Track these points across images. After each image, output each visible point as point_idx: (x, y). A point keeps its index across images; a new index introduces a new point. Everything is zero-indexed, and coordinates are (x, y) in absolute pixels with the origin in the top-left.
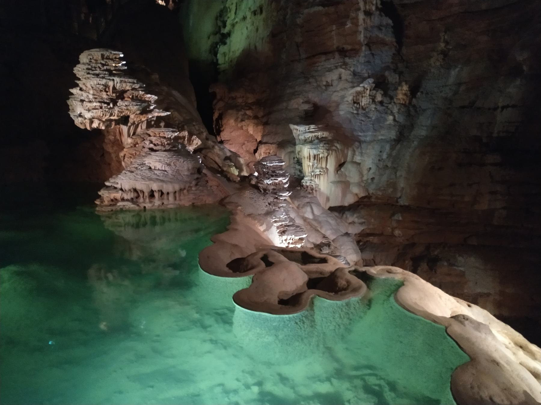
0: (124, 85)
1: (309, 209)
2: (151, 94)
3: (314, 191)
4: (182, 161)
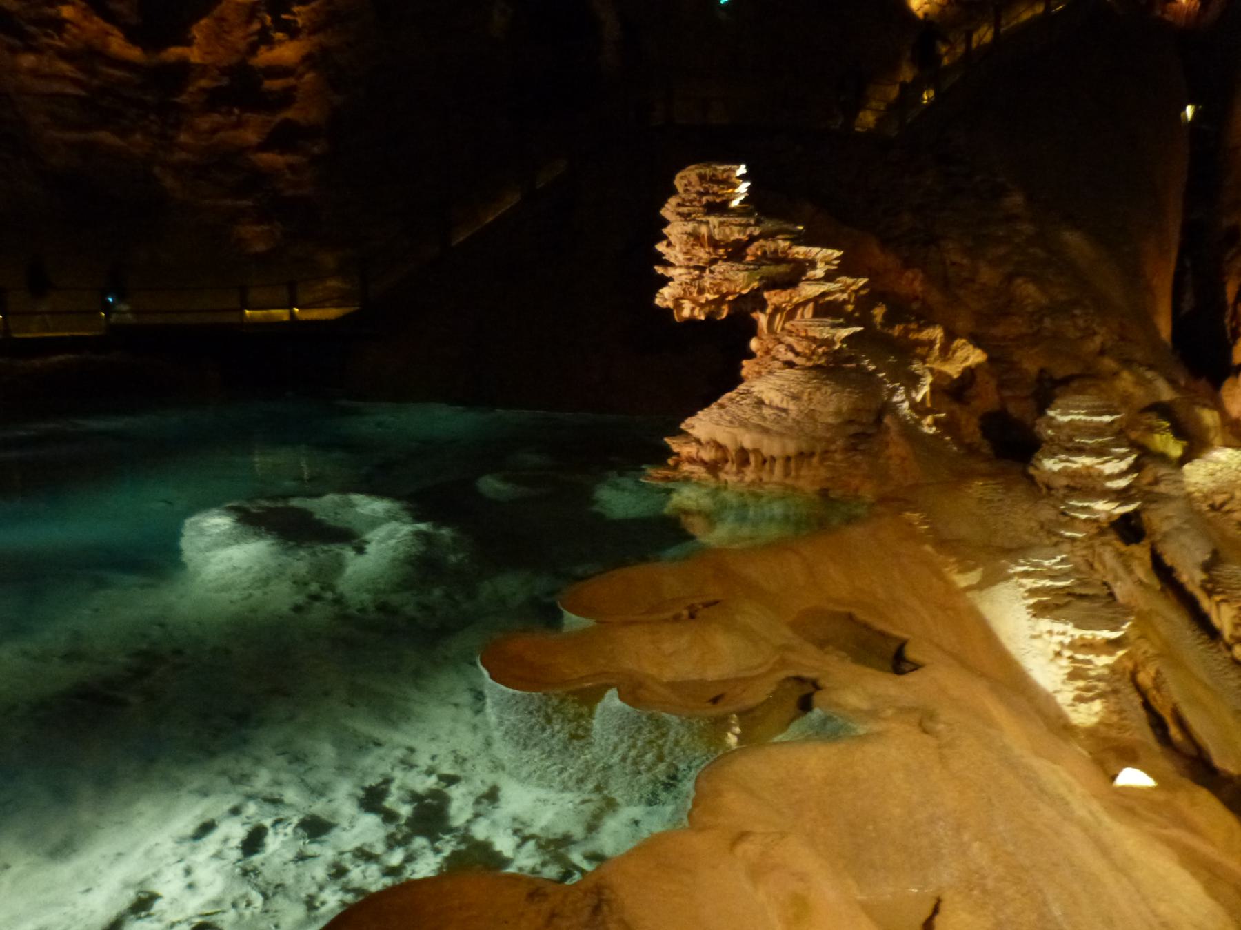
0: (727, 231)
4: (829, 391)
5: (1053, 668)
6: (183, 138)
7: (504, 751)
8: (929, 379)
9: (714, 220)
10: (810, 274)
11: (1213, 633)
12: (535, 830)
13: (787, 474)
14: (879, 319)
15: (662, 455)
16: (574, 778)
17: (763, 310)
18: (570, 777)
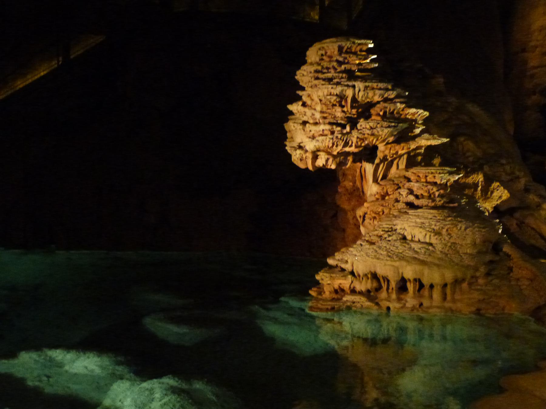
0: (371, 94)
2: (417, 107)
13: (444, 298)
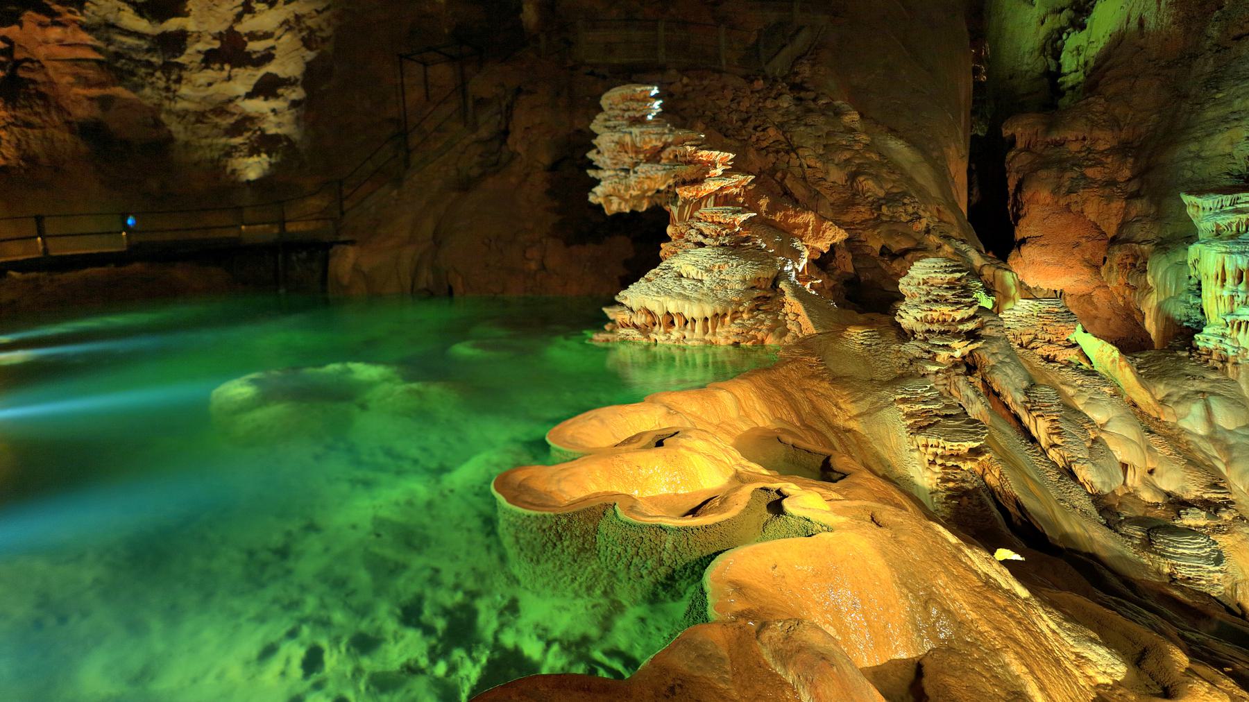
1: (1197, 409)
2: (710, 149)
3: (1229, 365)
5: (928, 474)
6: (184, 90)
7: (519, 568)
8: (806, 253)
9: (636, 130)
10: (712, 172)
11: (1033, 440)
12: (557, 633)
13: (706, 332)
14: (764, 208)
15: (600, 322)
16: (584, 585)
17: (674, 202)
18: (580, 585)
